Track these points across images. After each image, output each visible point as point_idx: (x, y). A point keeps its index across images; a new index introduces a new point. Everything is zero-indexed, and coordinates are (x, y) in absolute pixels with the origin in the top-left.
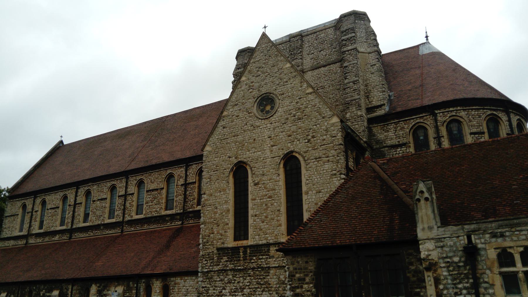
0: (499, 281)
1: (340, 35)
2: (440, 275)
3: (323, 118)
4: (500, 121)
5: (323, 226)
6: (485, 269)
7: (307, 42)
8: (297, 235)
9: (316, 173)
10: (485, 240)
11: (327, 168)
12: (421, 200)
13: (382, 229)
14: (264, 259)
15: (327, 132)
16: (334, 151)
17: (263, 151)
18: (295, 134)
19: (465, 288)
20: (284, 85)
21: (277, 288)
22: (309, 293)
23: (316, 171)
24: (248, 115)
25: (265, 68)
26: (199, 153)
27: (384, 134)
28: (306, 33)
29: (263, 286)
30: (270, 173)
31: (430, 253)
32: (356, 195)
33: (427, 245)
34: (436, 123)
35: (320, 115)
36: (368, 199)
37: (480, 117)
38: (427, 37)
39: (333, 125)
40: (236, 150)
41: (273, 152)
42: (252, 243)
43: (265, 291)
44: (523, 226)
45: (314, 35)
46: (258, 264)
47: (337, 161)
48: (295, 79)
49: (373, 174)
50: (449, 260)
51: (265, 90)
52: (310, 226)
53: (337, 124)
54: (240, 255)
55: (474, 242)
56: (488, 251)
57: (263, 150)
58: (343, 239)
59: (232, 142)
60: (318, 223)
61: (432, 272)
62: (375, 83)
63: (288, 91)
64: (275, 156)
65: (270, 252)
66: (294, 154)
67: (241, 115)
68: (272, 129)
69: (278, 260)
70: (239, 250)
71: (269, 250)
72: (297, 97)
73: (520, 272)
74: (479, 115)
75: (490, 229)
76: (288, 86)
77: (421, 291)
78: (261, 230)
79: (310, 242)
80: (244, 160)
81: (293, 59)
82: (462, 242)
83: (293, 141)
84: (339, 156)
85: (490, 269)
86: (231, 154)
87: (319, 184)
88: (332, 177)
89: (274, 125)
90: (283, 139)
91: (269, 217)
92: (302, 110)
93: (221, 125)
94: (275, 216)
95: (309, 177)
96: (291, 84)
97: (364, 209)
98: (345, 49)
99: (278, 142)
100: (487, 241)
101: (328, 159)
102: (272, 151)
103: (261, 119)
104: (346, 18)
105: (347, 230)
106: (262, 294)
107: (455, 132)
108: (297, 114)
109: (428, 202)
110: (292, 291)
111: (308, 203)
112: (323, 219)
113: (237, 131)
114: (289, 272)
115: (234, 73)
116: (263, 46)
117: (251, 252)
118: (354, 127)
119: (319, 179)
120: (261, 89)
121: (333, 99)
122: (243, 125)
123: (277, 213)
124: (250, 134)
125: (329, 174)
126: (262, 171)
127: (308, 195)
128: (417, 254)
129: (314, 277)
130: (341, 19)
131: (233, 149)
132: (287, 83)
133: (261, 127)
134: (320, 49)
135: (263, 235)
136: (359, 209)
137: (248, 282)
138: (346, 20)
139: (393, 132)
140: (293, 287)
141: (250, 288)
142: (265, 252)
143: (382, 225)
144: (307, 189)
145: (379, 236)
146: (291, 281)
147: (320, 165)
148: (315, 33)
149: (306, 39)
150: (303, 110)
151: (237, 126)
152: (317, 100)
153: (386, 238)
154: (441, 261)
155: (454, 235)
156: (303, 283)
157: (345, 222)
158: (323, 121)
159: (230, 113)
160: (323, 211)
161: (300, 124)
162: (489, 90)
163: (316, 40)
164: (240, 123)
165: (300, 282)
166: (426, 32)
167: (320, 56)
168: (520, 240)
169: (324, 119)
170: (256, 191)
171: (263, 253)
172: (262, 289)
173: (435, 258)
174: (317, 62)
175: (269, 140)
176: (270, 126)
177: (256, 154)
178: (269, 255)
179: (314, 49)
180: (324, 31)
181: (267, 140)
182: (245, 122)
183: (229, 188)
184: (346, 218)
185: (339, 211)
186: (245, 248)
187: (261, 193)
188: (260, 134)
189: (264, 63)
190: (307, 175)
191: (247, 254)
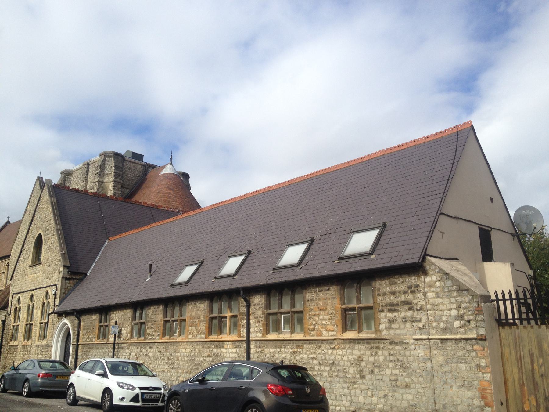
26: (9, 254)
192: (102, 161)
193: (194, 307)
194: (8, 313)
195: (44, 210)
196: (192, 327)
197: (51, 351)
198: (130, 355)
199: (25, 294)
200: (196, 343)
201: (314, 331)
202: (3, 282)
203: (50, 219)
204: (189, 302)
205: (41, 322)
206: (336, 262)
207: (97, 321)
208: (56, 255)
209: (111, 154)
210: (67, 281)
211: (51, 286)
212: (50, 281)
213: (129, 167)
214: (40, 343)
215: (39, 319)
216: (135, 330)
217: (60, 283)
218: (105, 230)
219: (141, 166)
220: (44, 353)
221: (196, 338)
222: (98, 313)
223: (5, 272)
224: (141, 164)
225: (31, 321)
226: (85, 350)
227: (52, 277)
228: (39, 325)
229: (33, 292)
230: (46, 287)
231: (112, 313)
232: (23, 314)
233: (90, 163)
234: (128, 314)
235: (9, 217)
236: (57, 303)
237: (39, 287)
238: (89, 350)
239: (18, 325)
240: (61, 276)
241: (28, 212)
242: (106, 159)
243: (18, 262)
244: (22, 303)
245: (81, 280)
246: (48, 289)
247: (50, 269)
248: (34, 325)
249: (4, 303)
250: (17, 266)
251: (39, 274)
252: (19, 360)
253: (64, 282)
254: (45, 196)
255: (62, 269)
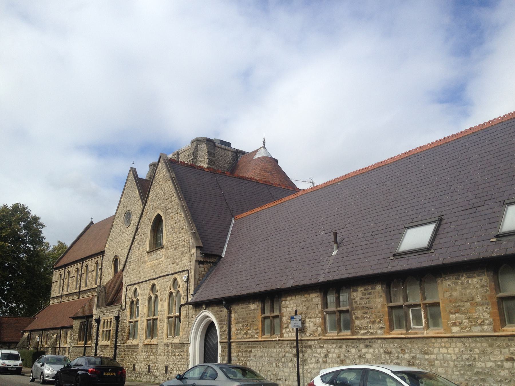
26: (103, 250)
38: (264, 142)
192: (194, 147)
193: (456, 284)
194: (121, 308)
195: (162, 188)
196: (457, 315)
197: (187, 351)
198: (326, 356)
199: (144, 285)
200: (470, 340)
201: (484, 325)
202: (93, 280)
203: (171, 195)
204: (441, 277)
205: (169, 315)
206: (492, 240)
207: (259, 311)
208: (184, 235)
209: (203, 140)
210: (201, 265)
211: (180, 272)
212: (178, 267)
213: (220, 154)
214: (170, 341)
215: (166, 312)
216: (328, 322)
217: (193, 268)
218: (229, 208)
219: (231, 153)
220: (177, 354)
221: (470, 331)
222: (259, 301)
223: (94, 271)
224: (232, 150)
225: (154, 315)
226: (243, 348)
227: (181, 261)
228: (166, 320)
229: (155, 282)
230: (172, 274)
231: (283, 299)
232: (143, 308)
233: (179, 152)
234: (314, 300)
235: (92, 218)
236: (191, 292)
237: (163, 274)
238: (249, 350)
239: (137, 321)
240: (194, 259)
241: (122, 205)
242: (199, 146)
243: (131, 249)
244: (140, 295)
245: (215, 264)
246: (176, 276)
247: (178, 253)
248: (160, 320)
249: (110, 298)
250: (130, 253)
251: (161, 260)
252: (142, 362)
253: (198, 266)
254: (161, 172)
255: (194, 251)
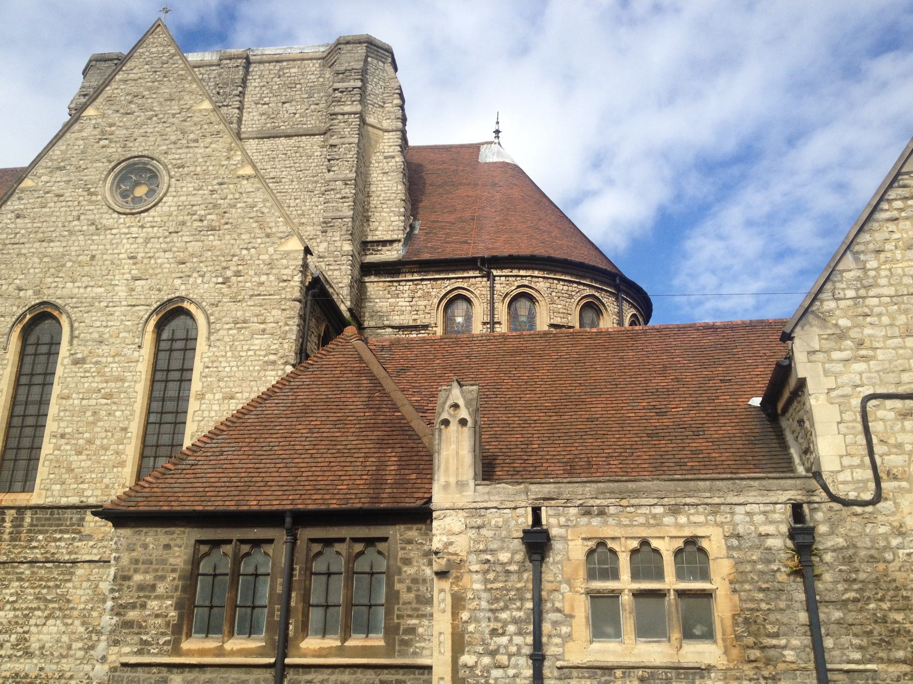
0: (583, 609)
1: (331, 79)
2: (465, 589)
3: (268, 236)
4: (604, 311)
5: (225, 466)
6: (560, 582)
7: (257, 77)
8: (154, 481)
9: (229, 354)
10: (568, 520)
11: (257, 347)
12: (451, 424)
13: (358, 482)
14: (65, 540)
15: (272, 268)
16: (280, 312)
17: (110, 288)
18: (195, 260)
19: (515, 621)
20: (188, 147)
21: (85, 612)
22: (159, 621)
23: (231, 350)
24: (87, 198)
25: (150, 101)
27: (389, 300)
28: (258, 57)
29: (51, 605)
30: (119, 340)
31: (453, 538)
32: (313, 404)
33: (448, 520)
34: (492, 294)
35: (261, 229)
36: (339, 415)
37: (571, 297)
38: (497, 132)
39: (287, 254)
40: (41, 275)
41: (133, 293)
42: (41, 502)
43: (54, 617)
44: (644, 496)
45: (275, 66)
46: (46, 552)
47: (283, 336)
48: (215, 139)
49: (356, 365)
50: (489, 557)
51: (141, 149)
52: (190, 462)
53: (296, 255)
54: (5, 527)
55: (544, 522)
56: (570, 543)
57: (111, 285)
58: (264, 498)
59: (34, 253)
60: (212, 458)
61: (451, 580)
62: (388, 195)
63: (194, 162)
64: (138, 302)
65: (83, 526)
66: (186, 305)
67: (68, 194)
68: (140, 240)
69: (100, 544)
70: (4, 513)
71: (83, 519)
72: (215, 178)
73: (626, 592)
74: (570, 293)
75: (580, 497)
76: (196, 150)
77: (420, 623)
78: (70, 470)
79: (185, 499)
80: (58, 301)
81: (221, 104)
82: (521, 520)
83: (189, 276)
84: (288, 325)
85: (568, 582)
86: (26, 282)
87: (232, 379)
88: (266, 368)
89: (148, 233)
90: (165, 268)
91: (98, 442)
92: (221, 211)
93: (12, 208)
94: (113, 441)
95: (213, 362)
96: (207, 147)
97: (325, 434)
98: (337, 110)
99: (151, 271)
100: (572, 521)
101: (262, 326)
102: (133, 290)
103: (119, 213)
104: (349, 47)
105: (278, 479)
106: (44, 624)
107: (523, 319)
108: (209, 217)
109: (465, 429)
110: (118, 614)
111: (201, 419)
112: (226, 449)
113: (52, 229)
114: (118, 569)
115: (73, 106)
116: (154, 50)
117: (35, 522)
118: (330, 273)
119: (234, 369)
120: (131, 145)
121: (297, 210)
122: (70, 218)
123: (119, 435)
124: (82, 243)
125: (259, 360)
126: (98, 332)
127: (203, 401)
128: (424, 542)
129: (180, 583)
130: (339, 46)
131: (32, 271)
132: (196, 145)
133: (114, 231)
134: (284, 98)
135: (74, 483)
136: (315, 435)
137: (11, 595)
138: (349, 52)
139: (406, 300)
140: (121, 605)
141: (15, 609)
142: (72, 525)
143: (359, 473)
144: (203, 387)
145: (348, 496)
146: (118, 591)
147: (242, 338)
148: (277, 61)
149: (256, 69)
150: (224, 210)
151: (54, 219)
152: (260, 196)
153: (363, 500)
154: (473, 558)
155: (506, 503)
156: (149, 597)
157: (277, 461)
158: (265, 243)
159: (40, 184)
160: (231, 433)
161: (212, 239)
162: (594, 252)
163: (279, 77)
164: (63, 214)
165: (141, 594)
166: (498, 123)
167: (281, 112)
168: (635, 525)
169: (268, 240)
170: (75, 379)
171: (67, 526)
172: (47, 613)
173: (461, 551)
174: (273, 124)
175: (129, 264)
176: (138, 233)
177: (92, 291)
178: (80, 532)
179: (271, 95)
180: (299, 62)
181: (125, 264)
182: (75, 213)
183: (5, 362)
184: (280, 452)
185: (267, 436)
186: (21, 510)
187: (86, 385)
188: (108, 247)
189: (149, 89)
190: (208, 357)
191: (21, 526)
